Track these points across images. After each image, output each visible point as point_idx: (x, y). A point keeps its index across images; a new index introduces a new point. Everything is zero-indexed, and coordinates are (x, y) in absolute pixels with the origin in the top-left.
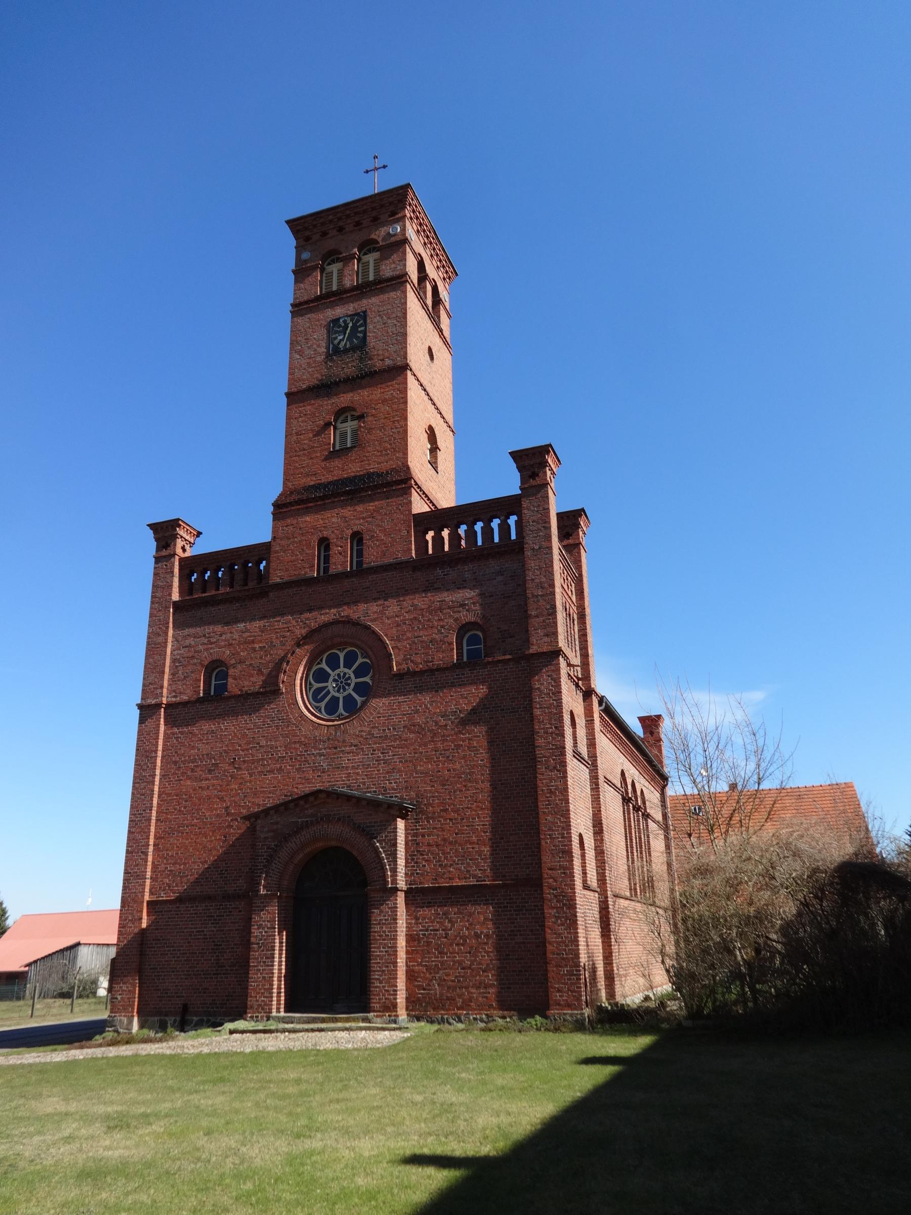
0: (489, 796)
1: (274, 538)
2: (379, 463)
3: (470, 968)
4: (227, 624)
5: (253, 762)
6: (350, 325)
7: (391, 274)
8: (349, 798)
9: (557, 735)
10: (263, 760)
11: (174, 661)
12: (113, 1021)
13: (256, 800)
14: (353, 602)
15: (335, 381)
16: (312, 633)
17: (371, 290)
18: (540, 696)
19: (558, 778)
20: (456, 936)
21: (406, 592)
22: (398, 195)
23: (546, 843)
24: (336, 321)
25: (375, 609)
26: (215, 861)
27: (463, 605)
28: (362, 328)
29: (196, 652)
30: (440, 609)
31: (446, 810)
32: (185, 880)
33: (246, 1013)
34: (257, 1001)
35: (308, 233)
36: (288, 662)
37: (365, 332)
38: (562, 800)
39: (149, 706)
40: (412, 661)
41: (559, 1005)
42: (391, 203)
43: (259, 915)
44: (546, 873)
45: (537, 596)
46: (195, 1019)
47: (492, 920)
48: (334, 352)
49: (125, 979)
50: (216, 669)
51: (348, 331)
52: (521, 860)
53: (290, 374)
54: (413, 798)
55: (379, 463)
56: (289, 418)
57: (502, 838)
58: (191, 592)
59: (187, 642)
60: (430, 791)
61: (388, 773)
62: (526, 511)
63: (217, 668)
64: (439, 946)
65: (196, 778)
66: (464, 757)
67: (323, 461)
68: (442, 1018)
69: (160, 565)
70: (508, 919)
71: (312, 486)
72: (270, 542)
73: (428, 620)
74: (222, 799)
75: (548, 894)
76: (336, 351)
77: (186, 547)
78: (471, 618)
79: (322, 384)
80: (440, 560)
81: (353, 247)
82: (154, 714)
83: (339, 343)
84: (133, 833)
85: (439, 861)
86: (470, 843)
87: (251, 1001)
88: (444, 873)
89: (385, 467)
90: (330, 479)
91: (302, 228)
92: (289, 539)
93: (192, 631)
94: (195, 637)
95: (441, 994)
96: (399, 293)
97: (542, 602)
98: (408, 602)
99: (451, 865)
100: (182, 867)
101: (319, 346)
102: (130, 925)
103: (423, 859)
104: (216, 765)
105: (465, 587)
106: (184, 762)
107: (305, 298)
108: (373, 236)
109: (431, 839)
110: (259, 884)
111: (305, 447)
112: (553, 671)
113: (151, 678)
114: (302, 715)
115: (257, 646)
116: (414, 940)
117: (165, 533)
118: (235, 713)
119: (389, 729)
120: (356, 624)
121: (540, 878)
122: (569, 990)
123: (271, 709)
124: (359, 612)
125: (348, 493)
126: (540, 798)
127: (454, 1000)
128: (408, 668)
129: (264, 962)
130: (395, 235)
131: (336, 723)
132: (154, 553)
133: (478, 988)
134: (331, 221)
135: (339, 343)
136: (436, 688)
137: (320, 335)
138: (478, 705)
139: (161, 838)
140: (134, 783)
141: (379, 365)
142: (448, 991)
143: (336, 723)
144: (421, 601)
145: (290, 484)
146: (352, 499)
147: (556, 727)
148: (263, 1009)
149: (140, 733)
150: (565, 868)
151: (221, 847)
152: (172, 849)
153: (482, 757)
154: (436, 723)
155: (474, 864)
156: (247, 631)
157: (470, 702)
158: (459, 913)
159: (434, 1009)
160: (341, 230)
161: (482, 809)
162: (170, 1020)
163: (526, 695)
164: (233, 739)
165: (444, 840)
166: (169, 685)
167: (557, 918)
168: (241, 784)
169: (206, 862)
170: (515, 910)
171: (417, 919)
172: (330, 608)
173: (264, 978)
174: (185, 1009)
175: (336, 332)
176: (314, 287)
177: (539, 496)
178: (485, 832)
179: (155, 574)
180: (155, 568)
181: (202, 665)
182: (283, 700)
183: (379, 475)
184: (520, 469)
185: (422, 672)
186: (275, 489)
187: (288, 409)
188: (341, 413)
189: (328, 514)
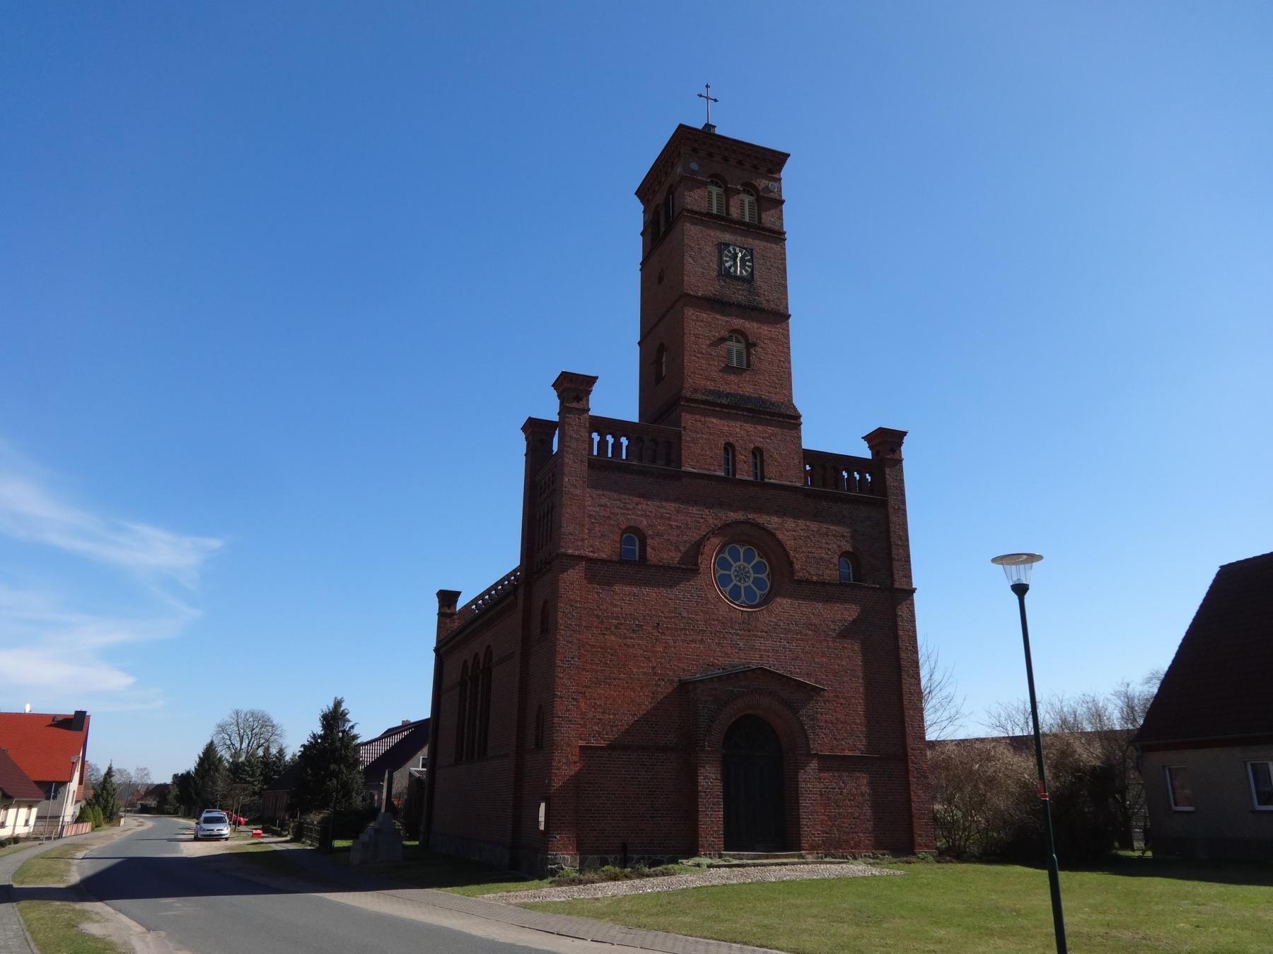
23: (909, 730)
24: (727, 245)
37: (752, 268)
59: (604, 501)
74: (648, 659)
87: (702, 841)
89: (774, 398)
107: (695, 208)
120: (761, 528)
121: (906, 755)
124: (772, 522)
125: (748, 410)
136: (827, 599)
141: (764, 305)
144: (814, 526)
162: (611, 858)
163: (894, 617)
174: (624, 847)
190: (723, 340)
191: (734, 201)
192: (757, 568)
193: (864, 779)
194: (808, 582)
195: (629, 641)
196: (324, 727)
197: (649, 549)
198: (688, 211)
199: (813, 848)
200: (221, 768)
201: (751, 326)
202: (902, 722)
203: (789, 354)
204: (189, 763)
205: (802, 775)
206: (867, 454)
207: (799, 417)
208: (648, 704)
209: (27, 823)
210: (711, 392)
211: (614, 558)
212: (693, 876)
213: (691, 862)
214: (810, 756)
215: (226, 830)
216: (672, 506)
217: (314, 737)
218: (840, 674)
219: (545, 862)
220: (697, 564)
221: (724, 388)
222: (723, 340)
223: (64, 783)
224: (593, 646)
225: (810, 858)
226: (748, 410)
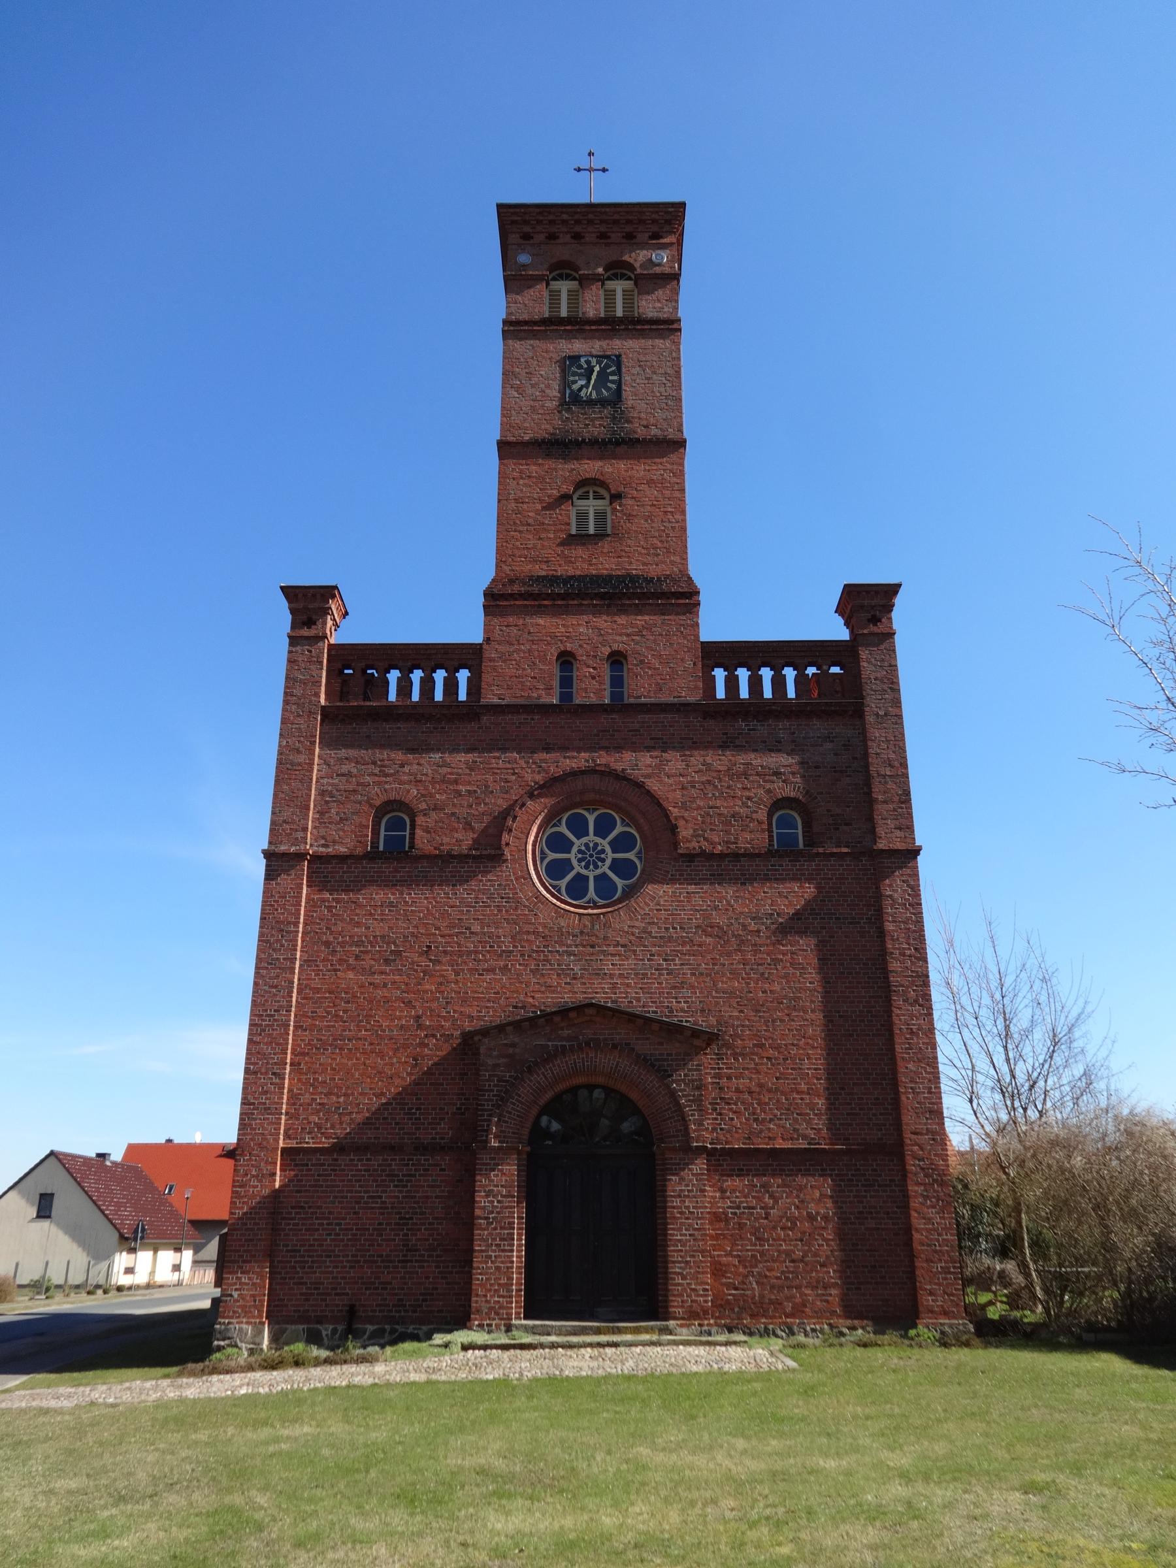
0: (823, 1031)
1: (487, 640)
2: (645, 564)
3: (802, 1261)
4: (412, 750)
5: (460, 954)
6: (597, 369)
7: (656, 314)
8: (632, 1017)
9: (919, 959)
10: (476, 952)
11: (322, 793)
12: (227, 1330)
13: (467, 1010)
14: (615, 748)
15: (577, 440)
17: (627, 329)
18: (892, 906)
19: (921, 1014)
20: (782, 1217)
21: (695, 745)
22: (667, 213)
23: (907, 1099)
24: (575, 359)
25: (649, 761)
26: (399, 1093)
27: (777, 774)
28: (615, 378)
29: (359, 784)
30: (745, 774)
31: (761, 1046)
32: (347, 1119)
33: (469, 1319)
34: (487, 1301)
35: (527, 229)
36: (515, 817)
37: (619, 384)
38: (927, 1044)
39: (284, 855)
40: (706, 839)
41: (932, 1312)
42: (654, 221)
43: (488, 1177)
44: (908, 1137)
45: (884, 776)
46: (370, 1328)
47: (831, 1197)
48: (571, 401)
49: (247, 1266)
50: (395, 813)
51: (594, 377)
52: (870, 1119)
53: (503, 415)
54: (712, 1026)
55: (645, 564)
56: (502, 476)
57: (843, 1089)
58: (343, 696)
59: (345, 769)
60: (738, 1018)
61: (674, 987)
62: (865, 664)
63: (394, 811)
64: (757, 1229)
65: (364, 969)
66: (786, 976)
67: (558, 545)
68: (766, 1329)
69: (298, 648)
70: (855, 1197)
71: (544, 577)
72: (481, 645)
73: (728, 787)
74: (409, 1004)
75: (912, 1165)
76: (576, 399)
77: (345, 632)
78: (789, 792)
79: (557, 441)
80: (733, 709)
81: (597, 266)
82: (293, 867)
83: (580, 390)
84: (255, 1043)
85: (754, 1114)
86: (798, 1093)
88: (761, 1131)
89: (653, 571)
91: (521, 225)
93: (352, 753)
94: (357, 763)
95: (762, 1296)
96: (668, 343)
97: (890, 785)
98: (697, 758)
99: (771, 1120)
100: (342, 1100)
101: (548, 386)
102: (254, 1182)
103: (731, 1109)
104: (398, 953)
105: (779, 751)
107: (526, 317)
108: (626, 258)
109: (743, 1083)
110: (488, 1131)
111: (530, 521)
112: (909, 875)
113: (286, 814)
114: (538, 895)
115: (463, 789)
116: (721, 1221)
117: (309, 605)
118: (429, 882)
119: (674, 928)
121: (901, 1144)
122: (945, 1292)
123: (489, 881)
124: (626, 761)
125: (602, 596)
126: (897, 1040)
127: (780, 1304)
128: (700, 847)
129: (498, 1245)
130: (659, 265)
131: (590, 911)
132: (288, 629)
133: (814, 1288)
134: (564, 222)
135: (580, 390)
136: (744, 880)
137: (549, 373)
138: (804, 908)
139: (303, 1054)
140: (257, 968)
141: (641, 433)
142: (771, 1292)
143: (590, 911)
144: (719, 760)
145: (507, 569)
146: (609, 606)
147: (916, 949)
148: (497, 1314)
149: (267, 893)
150: (934, 1133)
151: (410, 1074)
152: (324, 1071)
153: (811, 978)
154: (744, 926)
155: (804, 1120)
156: (445, 765)
157: (791, 904)
158: (784, 1185)
159: (752, 1316)
160: (577, 237)
161: (813, 1047)
162: (326, 1330)
164: (425, 917)
165: (761, 1086)
166: (314, 827)
167: (926, 1197)
168: (441, 984)
169: (383, 1094)
170: (863, 1185)
171: (723, 1191)
172: (579, 750)
173: (498, 1268)
175: (575, 374)
176: (535, 302)
177: (882, 647)
178: (818, 1079)
179: (291, 661)
180: (290, 652)
181: (371, 806)
182: (506, 871)
183: (648, 581)
184: (293, 611)
185: (722, 856)
186: (486, 574)
187: (501, 464)
188: (587, 485)
189: (572, 620)
190: (566, 497)
195: (378, 978)
197: (419, 832)
199: (693, 1315)
202: (895, 1084)
203: (682, 500)
205: (674, 1185)
206: (840, 632)
208: (406, 1077)
210: (539, 579)
211: (359, 851)
212: (443, 1362)
214: (690, 1152)
218: (777, 1007)
220: (499, 848)
222: (566, 497)
224: (318, 990)
225: (684, 1334)
226: (602, 596)
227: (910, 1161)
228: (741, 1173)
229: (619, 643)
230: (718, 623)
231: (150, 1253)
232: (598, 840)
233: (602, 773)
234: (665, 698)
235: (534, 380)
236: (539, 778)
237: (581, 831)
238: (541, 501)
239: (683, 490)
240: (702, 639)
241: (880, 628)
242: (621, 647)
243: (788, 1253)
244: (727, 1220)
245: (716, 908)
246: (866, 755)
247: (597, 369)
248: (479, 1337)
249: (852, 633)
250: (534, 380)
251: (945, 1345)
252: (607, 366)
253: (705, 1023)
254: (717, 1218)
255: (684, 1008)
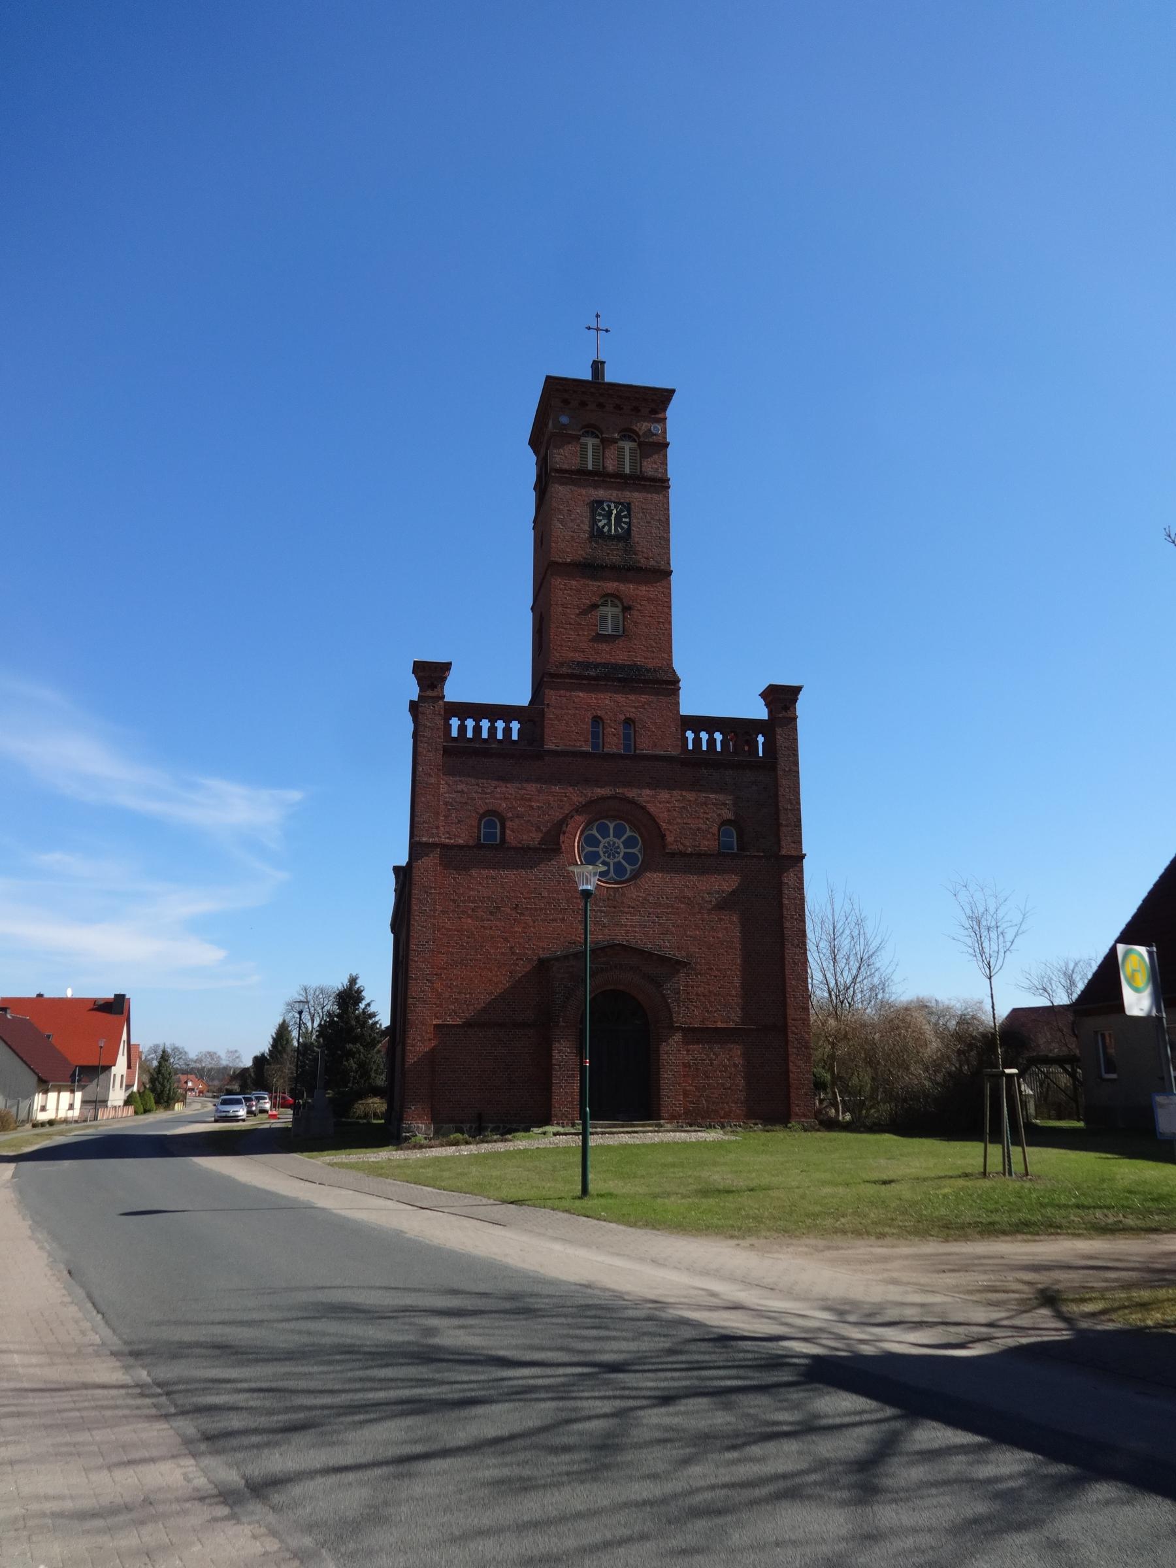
5: (536, 910)
6: (615, 512)
13: (541, 944)
16: (591, 802)
23: (790, 1001)
24: (600, 503)
30: (706, 804)
37: (629, 524)
48: (597, 535)
59: (460, 788)
74: (506, 940)
75: (791, 1037)
87: (554, 1111)
89: (651, 664)
90: (599, 661)
92: (562, 708)
106: (464, 902)
107: (566, 467)
109: (700, 990)
117: (431, 675)
120: (632, 802)
121: (785, 1026)
124: (643, 795)
125: (620, 680)
136: (703, 871)
144: (691, 796)
160: (601, 406)
162: (466, 1127)
163: (779, 887)
165: (710, 992)
171: (688, 1051)
175: (600, 514)
183: (648, 670)
185: (691, 854)
188: (612, 598)
190: (595, 606)
191: (611, 453)
192: (630, 843)
193: (737, 1051)
194: (683, 855)
195: (486, 923)
196: (340, 1006)
197: (508, 831)
198: (557, 471)
199: (672, 1117)
200: (289, 1049)
201: (627, 589)
204: (263, 1045)
205: (664, 1048)
207: (678, 681)
209: (71, 1107)
211: (471, 843)
213: (541, 1130)
214: (673, 1029)
215: (242, 1112)
216: (532, 787)
217: (329, 1014)
219: (399, 1130)
220: (558, 844)
221: (594, 658)
223: (107, 1068)
224: (450, 930)
225: (669, 1126)
226: (620, 680)
227: (790, 1035)
228: (698, 1042)
229: (631, 713)
230: (691, 704)
231: (56, 1094)
232: (616, 840)
233: (621, 799)
234: (660, 752)
235: (573, 516)
236: (582, 800)
237: (605, 835)
238: (579, 608)
239: (670, 608)
240: (682, 713)
241: (789, 714)
242: (632, 716)
243: (723, 1085)
244: (690, 1067)
245: (687, 887)
246: (776, 795)
247: (615, 512)
248: (561, 1130)
249: (770, 713)
250: (573, 516)
251: (805, 1131)
252: (621, 511)
253: (680, 956)
254: (685, 1065)
255: (667, 946)
